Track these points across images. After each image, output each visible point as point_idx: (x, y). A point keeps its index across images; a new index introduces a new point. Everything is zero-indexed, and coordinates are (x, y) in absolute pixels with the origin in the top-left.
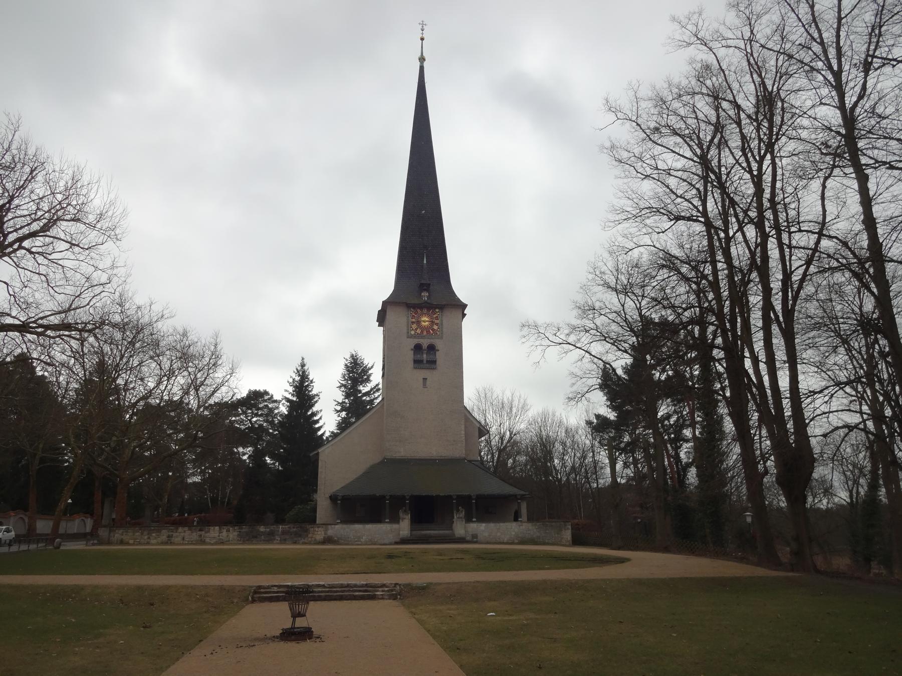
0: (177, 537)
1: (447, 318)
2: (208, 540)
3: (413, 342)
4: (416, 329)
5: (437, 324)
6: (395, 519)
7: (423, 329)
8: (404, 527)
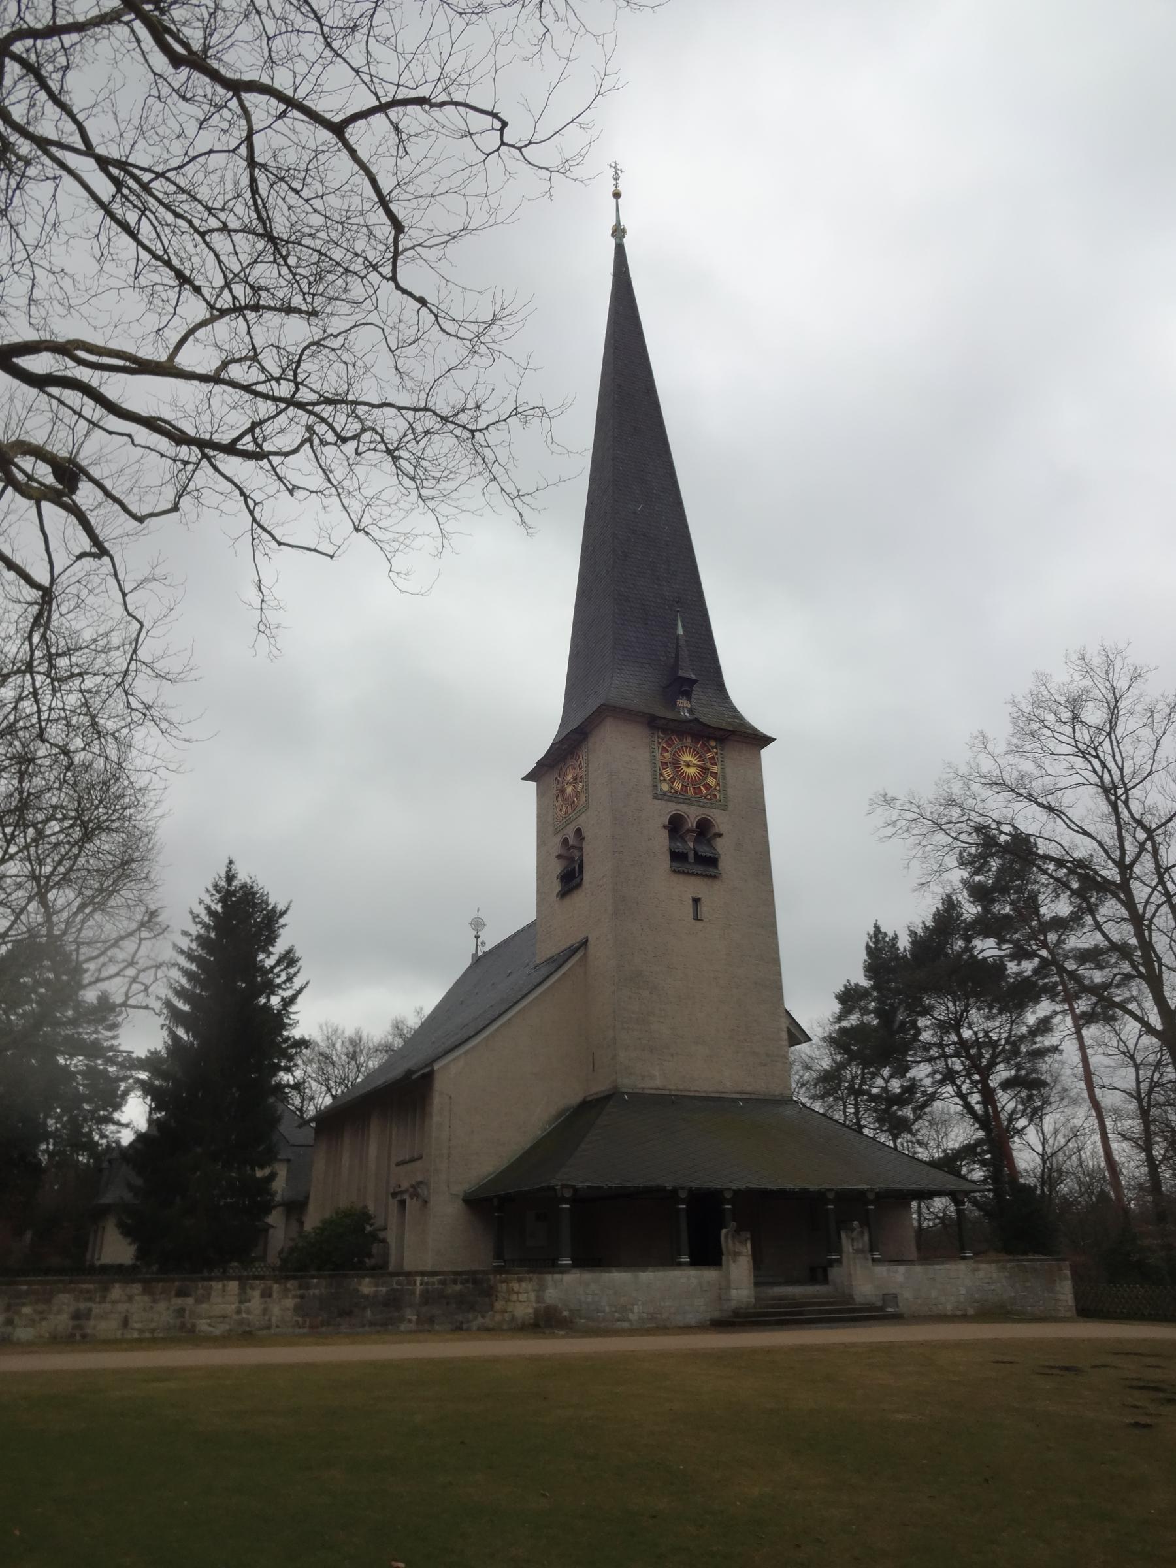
1: (731, 764)
2: (203, 1326)
3: (665, 811)
4: (672, 781)
5: (714, 775)
6: (707, 1254)
7: (687, 781)
8: (738, 1277)
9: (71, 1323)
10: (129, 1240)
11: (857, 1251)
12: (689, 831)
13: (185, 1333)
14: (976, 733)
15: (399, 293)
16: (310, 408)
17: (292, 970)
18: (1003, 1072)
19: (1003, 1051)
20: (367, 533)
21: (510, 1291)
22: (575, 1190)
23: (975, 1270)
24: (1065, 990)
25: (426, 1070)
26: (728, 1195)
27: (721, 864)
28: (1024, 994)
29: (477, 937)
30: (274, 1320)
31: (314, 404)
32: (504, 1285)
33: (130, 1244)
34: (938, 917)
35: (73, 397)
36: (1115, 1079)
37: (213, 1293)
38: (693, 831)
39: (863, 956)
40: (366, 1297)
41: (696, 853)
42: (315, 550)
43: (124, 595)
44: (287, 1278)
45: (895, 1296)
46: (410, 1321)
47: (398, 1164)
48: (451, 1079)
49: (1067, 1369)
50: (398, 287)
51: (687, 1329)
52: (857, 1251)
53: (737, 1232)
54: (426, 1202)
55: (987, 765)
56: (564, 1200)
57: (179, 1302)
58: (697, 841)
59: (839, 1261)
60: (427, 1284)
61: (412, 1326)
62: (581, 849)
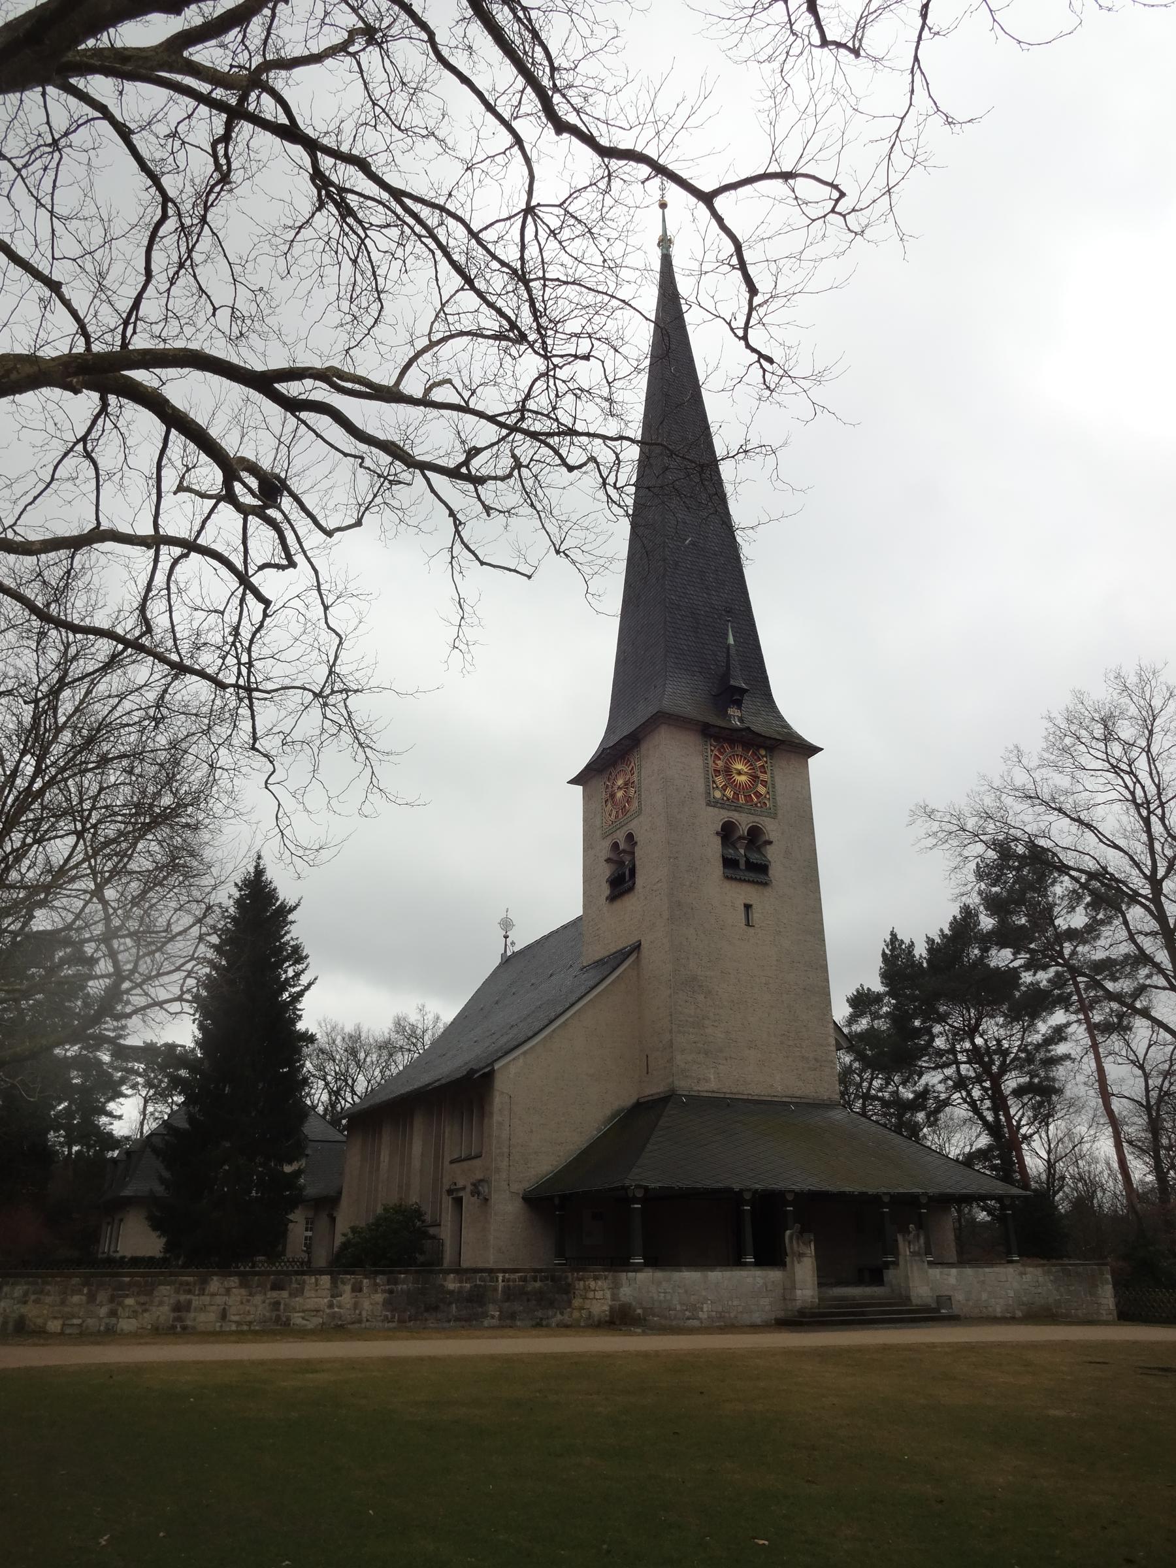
0: (203, 1309)
1: (780, 772)
2: (297, 1319)
3: (714, 819)
4: (724, 788)
5: (765, 783)
6: (771, 1255)
7: (738, 788)
9: (172, 1315)
10: (158, 1233)
11: (914, 1254)
12: (741, 838)
13: (279, 1326)
14: (1011, 747)
15: (748, 351)
16: (543, 438)
17: (300, 967)
18: (1011, 1082)
19: (1016, 1058)
20: (567, 556)
21: (587, 1289)
22: (646, 1189)
23: (1022, 1274)
24: (1081, 1000)
25: (486, 1070)
26: (790, 1197)
27: (771, 872)
28: (1037, 1003)
29: (506, 937)
30: (364, 1314)
31: (550, 435)
32: (582, 1283)
33: (159, 1237)
34: (955, 924)
35: (322, 422)
36: (1124, 1088)
37: (307, 1287)
38: (744, 838)
39: (879, 963)
40: (451, 1292)
41: (747, 862)
42: (515, 571)
43: (326, 608)
44: (377, 1273)
45: (950, 1298)
46: (493, 1317)
47: (452, 1162)
48: (513, 1081)
49: (1163, 1369)
50: (748, 346)
51: (754, 1328)
52: (914, 1254)
53: (802, 1232)
54: (486, 1200)
55: (1021, 779)
56: (635, 1200)
57: (275, 1294)
58: (747, 848)
59: (896, 1264)
60: (508, 1280)
61: (495, 1322)
62: (633, 853)
